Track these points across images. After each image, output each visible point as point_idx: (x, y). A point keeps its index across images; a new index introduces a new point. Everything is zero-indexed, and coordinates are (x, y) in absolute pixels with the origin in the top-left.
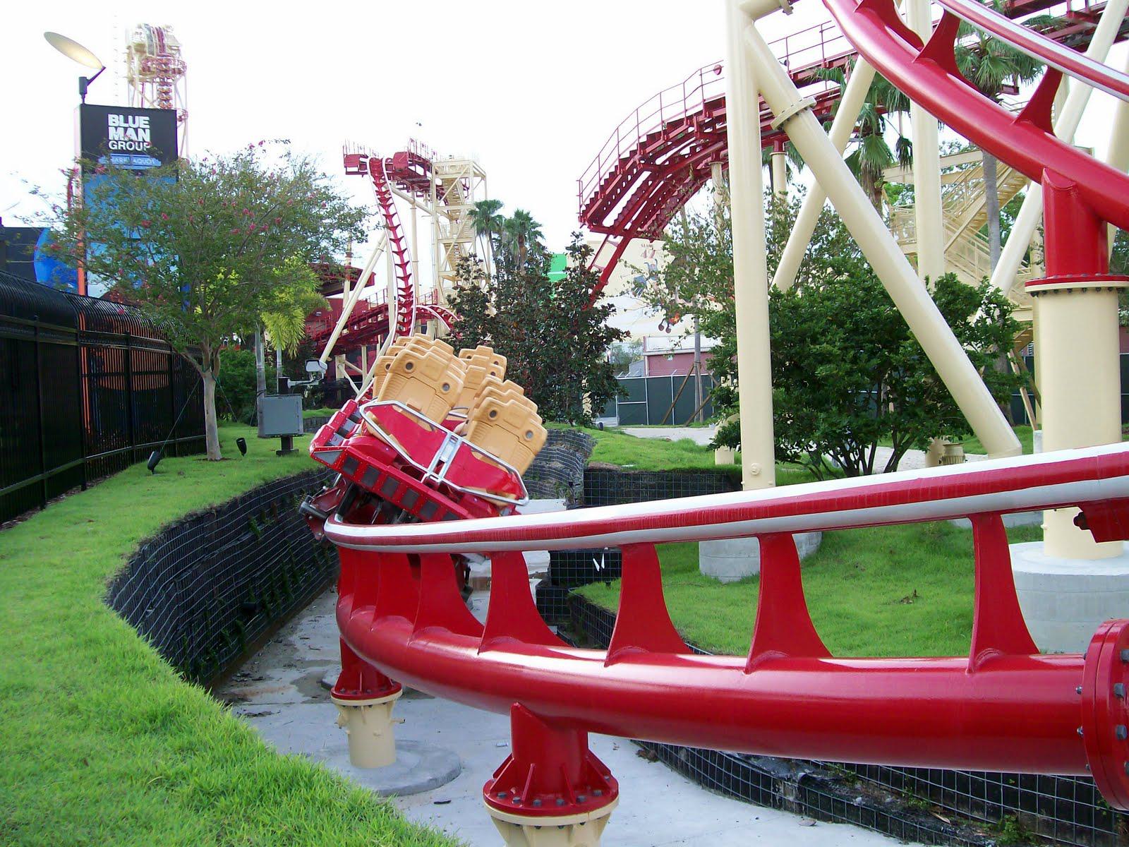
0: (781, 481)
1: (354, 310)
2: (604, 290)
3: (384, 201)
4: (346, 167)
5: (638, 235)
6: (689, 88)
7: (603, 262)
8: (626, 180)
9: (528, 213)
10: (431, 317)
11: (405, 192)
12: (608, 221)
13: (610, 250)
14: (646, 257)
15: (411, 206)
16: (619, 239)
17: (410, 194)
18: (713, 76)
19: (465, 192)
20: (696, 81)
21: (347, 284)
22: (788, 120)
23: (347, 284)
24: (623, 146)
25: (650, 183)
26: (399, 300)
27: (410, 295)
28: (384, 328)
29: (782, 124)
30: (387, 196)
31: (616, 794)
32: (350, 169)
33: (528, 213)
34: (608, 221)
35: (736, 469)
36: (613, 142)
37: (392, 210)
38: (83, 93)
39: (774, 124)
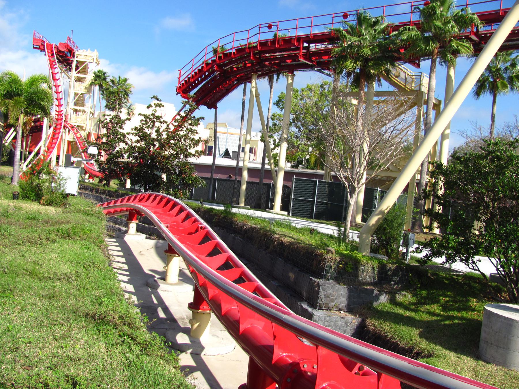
3: (52, 66)
4: (33, 44)
6: (252, 33)
18: (267, 29)
20: (257, 30)
32: (35, 46)
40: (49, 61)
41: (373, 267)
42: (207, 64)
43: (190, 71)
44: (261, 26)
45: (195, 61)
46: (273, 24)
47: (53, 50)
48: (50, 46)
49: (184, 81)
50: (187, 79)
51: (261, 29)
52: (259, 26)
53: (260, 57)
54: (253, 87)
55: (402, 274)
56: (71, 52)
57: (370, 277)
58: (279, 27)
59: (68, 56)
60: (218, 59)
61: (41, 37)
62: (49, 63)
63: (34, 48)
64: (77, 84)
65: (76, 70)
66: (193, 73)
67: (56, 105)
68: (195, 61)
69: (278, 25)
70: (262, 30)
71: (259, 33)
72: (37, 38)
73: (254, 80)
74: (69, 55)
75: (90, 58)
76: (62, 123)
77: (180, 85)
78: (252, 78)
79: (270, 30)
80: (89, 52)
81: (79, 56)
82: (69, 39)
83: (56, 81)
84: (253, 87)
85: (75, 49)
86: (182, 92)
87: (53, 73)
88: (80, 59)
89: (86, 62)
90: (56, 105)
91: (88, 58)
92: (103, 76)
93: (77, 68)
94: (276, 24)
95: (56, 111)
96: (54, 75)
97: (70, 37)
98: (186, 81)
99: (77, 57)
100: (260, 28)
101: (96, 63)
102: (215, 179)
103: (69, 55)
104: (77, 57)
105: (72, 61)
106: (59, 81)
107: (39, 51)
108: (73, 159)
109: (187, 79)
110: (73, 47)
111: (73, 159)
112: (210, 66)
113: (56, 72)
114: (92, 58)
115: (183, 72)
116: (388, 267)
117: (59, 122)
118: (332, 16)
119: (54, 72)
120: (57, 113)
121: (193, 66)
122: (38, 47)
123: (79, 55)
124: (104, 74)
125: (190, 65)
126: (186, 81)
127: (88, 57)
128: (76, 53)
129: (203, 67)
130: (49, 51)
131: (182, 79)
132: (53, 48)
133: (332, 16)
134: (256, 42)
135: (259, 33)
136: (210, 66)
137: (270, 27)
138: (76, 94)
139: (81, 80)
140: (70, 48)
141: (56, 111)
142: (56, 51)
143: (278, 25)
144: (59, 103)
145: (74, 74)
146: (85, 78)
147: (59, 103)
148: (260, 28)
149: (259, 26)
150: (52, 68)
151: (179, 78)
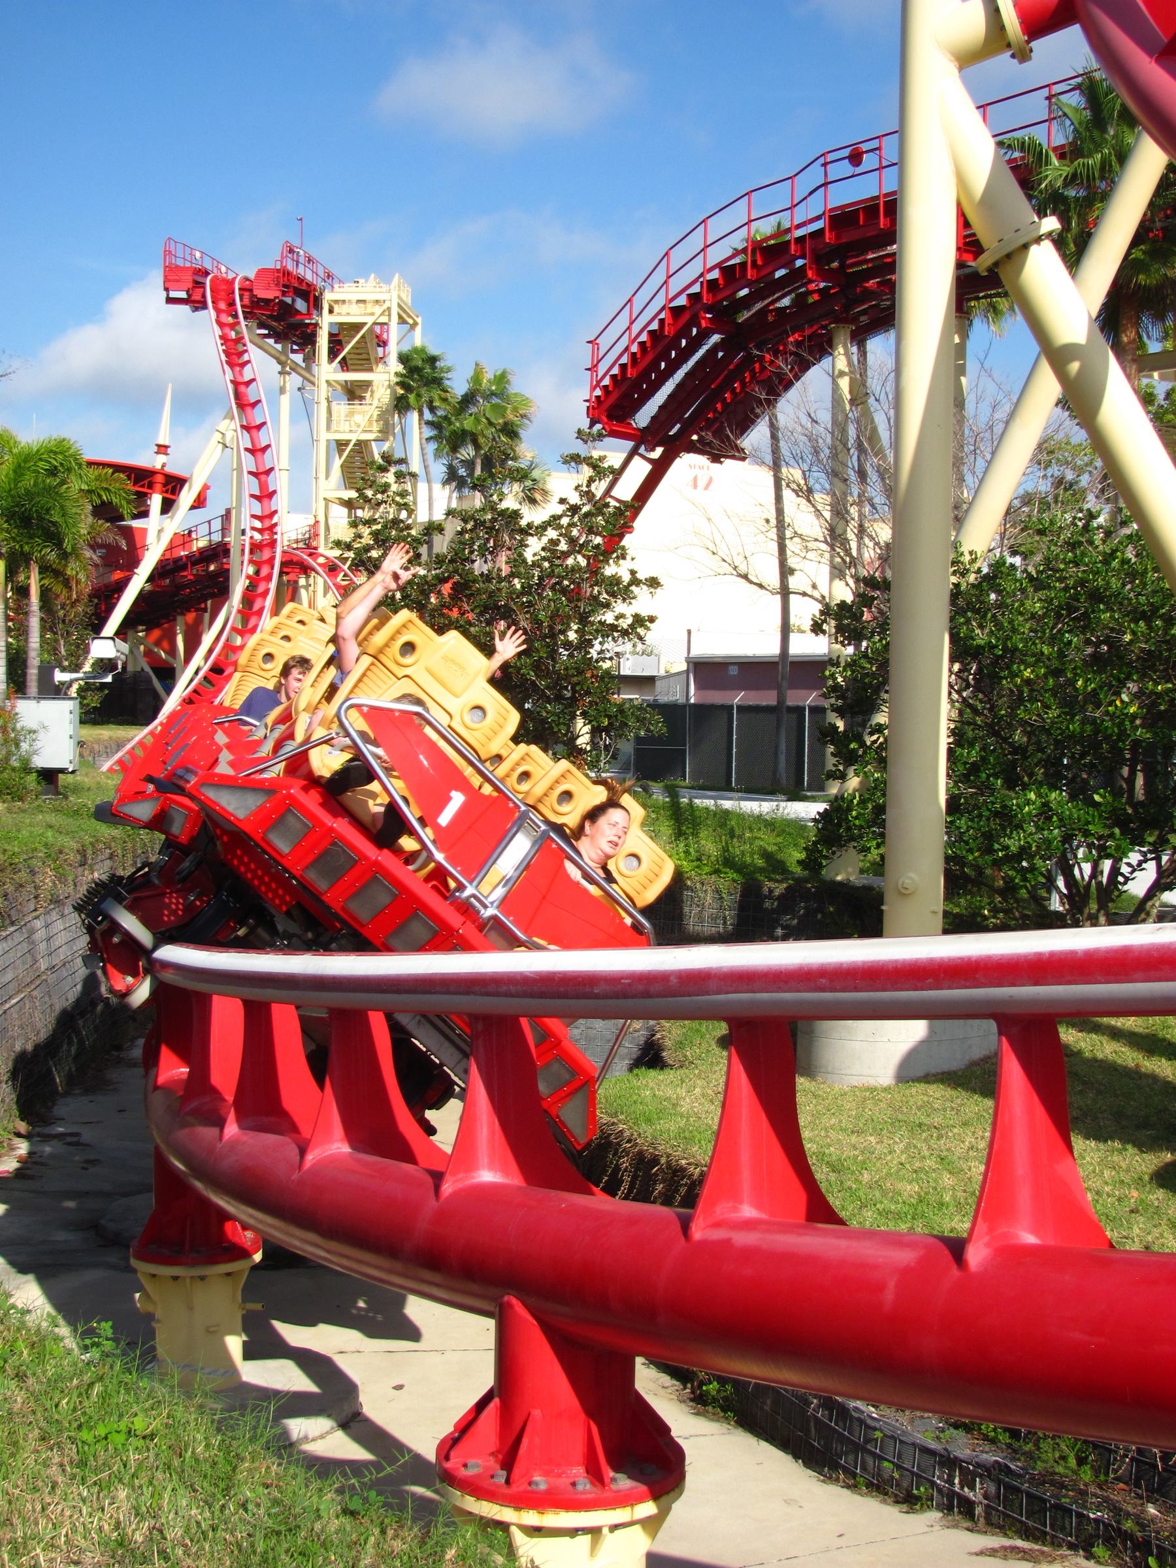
0: (956, 925)
1: (171, 547)
2: (627, 541)
3: (234, 355)
4: (167, 289)
5: (692, 448)
6: (802, 188)
7: (626, 489)
8: (677, 346)
9: (449, 370)
10: (306, 569)
11: (271, 341)
12: (643, 418)
13: (639, 469)
14: (695, 486)
15: (279, 368)
16: (658, 452)
17: (279, 347)
18: (846, 168)
19: (380, 350)
20: (815, 176)
21: (156, 501)
22: (1008, 256)
23: (156, 501)
24: (676, 284)
25: (720, 354)
26: (252, 538)
27: (272, 529)
28: (219, 588)
29: (996, 264)
30: (240, 348)
31: (14, 1074)
32: (173, 294)
33: (449, 370)
34: (643, 418)
35: (868, 889)
36: (659, 277)
37: (247, 374)
38: (803, 632)
39: (982, 264)
40: (219, 342)
41: (718, 891)
42: (676, 312)
43: (624, 342)
44: (830, 157)
45: (638, 305)
46: (865, 147)
47: (234, 300)
48: (224, 288)
49: (608, 378)
50: (615, 371)
51: (829, 167)
52: (822, 160)
53: (843, 266)
54: (842, 374)
55: (805, 908)
56: (312, 296)
57: (714, 918)
58: (884, 153)
59: (298, 312)
60: (709, 291)
61: (198, 255)
62: (221, 348)
63: (170, 300)
64: (341, 408)
65: (331, 358)
66: (634, 348)
67: (252, 496)
68: (638, 305)
69: (879, 149)
70: (835, 171)
71: (825, 184)
72: (180, 263)
73: (841, 350)
74: (301, 305)
75: (378, 310)
76: (273, 558)
77: (598, 392)
78: (835, 341)
79: (859, 170)
80: (369, 288)
81: (336, 308)
82: (291, 251)
83: (248, 409)
84: (842, 374)
85: (320, 283)
86: (608, 417)
87: (235, 383)
88: (348, 314)
89: (365, 324)
90: (252, 496)
91: (370, 308)
92: (428, 370)
93: (333, 354)
94: (874, 144)
95: (254, 516)
96: (242, 388)
97: (295, 242)
98: (613, 377)
99: (331, 311)
100: (825, 165)
101: (404, 322)
102: (800, 710)
103: (301, 305)
104: (331, 311)
105: (316, 325)
106: (258, 408)
107: (185, 309)
108: (60, 676)
109: (615, 371)
110: (309, 277)
111: (60, 676)
112: (686, 317)
113: (247, 378)
114: (385, 307)
115: (605, 342)
116: (765, 890)
117: (266, 554)
118: (1045, 92)
119: (240, 380)
120: (258, 524)
121: (632, 323)
122: (183, 295)
123: (336, 302)
124: (433, 360)
125: (623, 321)
126: (613, 377)
127: (369, 306)
128: (328, 296)
129: (662, 321)
130: (222, 306)
131: (602, 369)
132: (233, 292)
133: (1045, 92)
134: (818, 218)
135: (825, 184)
136: (686, 317)
137: (855, 157)
138: (341, 445)
139: (358, 392)
140: (301, 280)
141: (254, 516)
142: (247, 301)
143: (879, 149)
144: (263, 486)
145: (327, 371)
146: (367, 385)
147: (263, 486)
148: (825, 165)
149: (822, 160)
150: (231, 364)
151: (593, 369)
